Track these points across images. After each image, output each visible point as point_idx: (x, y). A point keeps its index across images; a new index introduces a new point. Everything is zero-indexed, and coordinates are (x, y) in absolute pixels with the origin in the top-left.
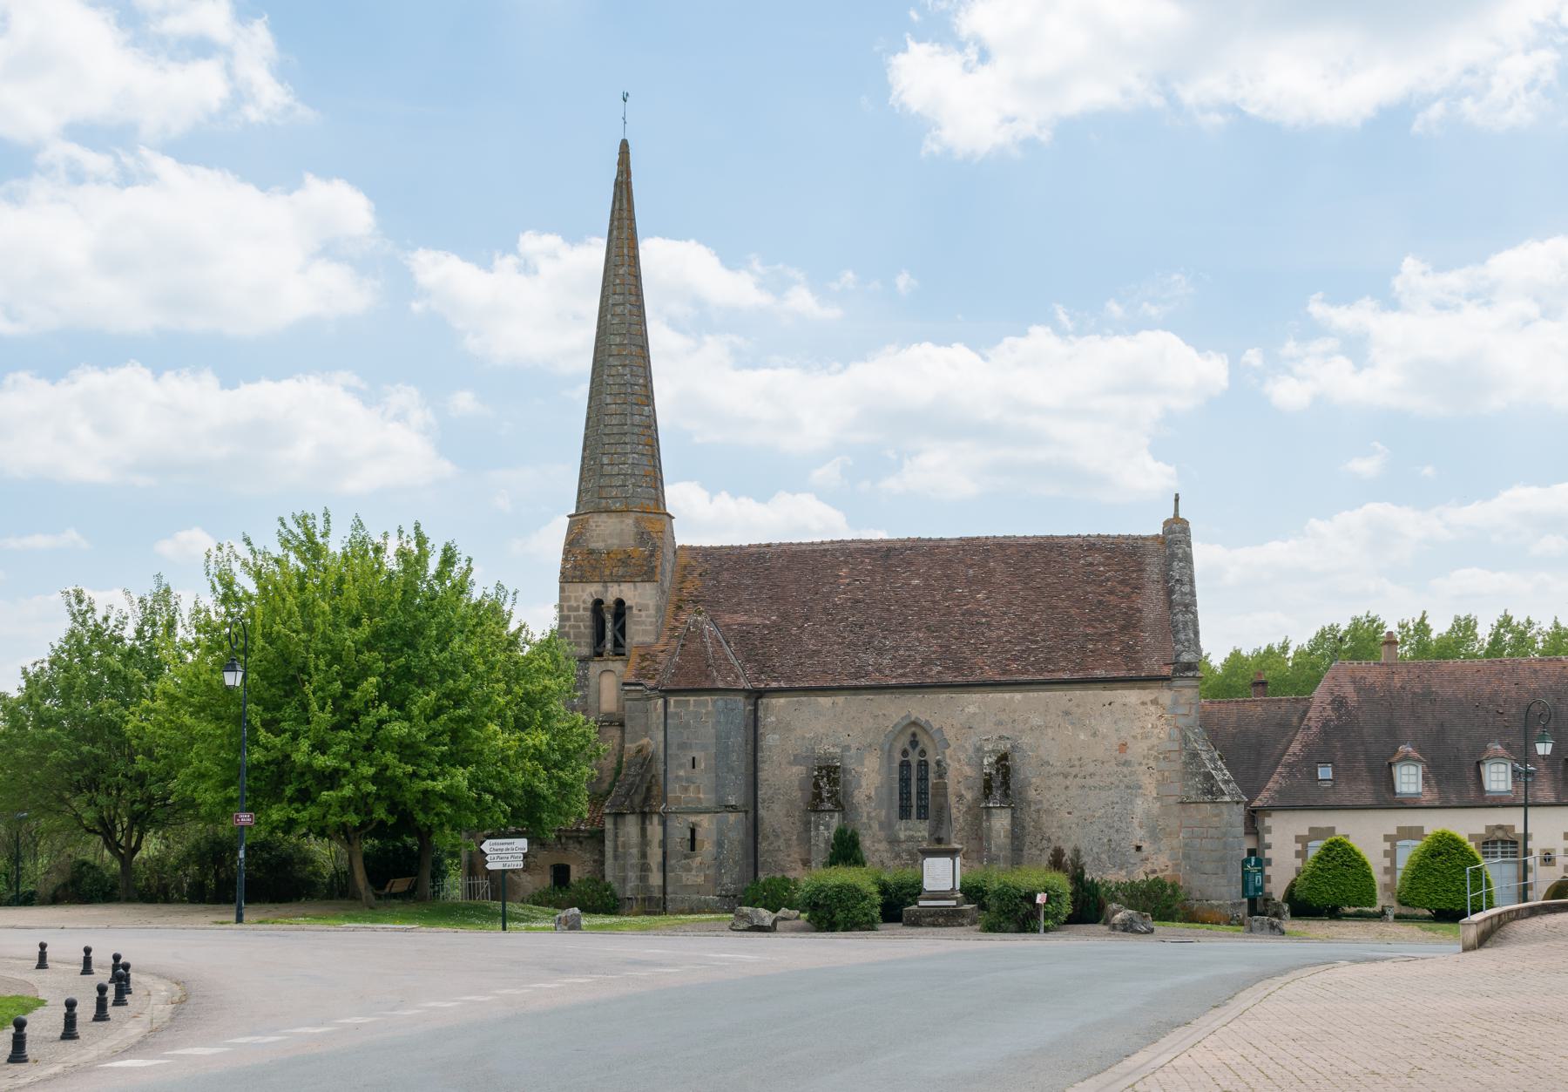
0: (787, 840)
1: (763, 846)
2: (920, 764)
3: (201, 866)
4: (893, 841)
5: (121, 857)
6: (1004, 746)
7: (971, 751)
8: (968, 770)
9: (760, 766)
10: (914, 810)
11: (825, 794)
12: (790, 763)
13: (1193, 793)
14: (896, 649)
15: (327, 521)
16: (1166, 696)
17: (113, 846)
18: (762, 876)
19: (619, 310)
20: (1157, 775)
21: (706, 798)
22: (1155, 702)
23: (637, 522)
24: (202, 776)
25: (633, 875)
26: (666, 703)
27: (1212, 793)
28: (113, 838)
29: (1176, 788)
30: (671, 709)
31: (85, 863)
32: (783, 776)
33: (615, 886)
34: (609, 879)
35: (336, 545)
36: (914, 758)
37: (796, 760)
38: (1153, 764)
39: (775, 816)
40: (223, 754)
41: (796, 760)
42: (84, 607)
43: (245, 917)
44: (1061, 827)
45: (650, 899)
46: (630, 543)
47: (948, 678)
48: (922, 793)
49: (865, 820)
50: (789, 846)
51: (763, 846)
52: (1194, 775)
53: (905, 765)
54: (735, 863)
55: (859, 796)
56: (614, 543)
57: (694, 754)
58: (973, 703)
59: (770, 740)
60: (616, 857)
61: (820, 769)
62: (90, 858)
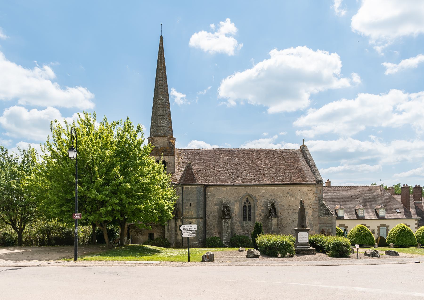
0: (214, 227)
1: (207, 228)
2: (249, 206)
3: (43, 234)
4: (243, 227)
5: (18, 232)
6: (272, 202)
7: (263, 202)
8: (262, 208)
9: (206, 206)
10: (247, 219)
11: (226, 214)
12: (215, 206)
13: (322, 215)
14: (241, 175)
15: (95, 116)
16: (314, 189)
17: (16, 229)
18: (207, 237)
19: (161, 82)
20: (312, 210)
21: (194, 215)
22: (311, 190)
23: (168, 140)
24: (50, 203)
25: (173, 236)
26: (182, 188)
27: (328, 214)
28: (15, 226)
29: (317, 213)
30: (184, 190)
31: (6, 234)
32: (213, 209)
33: (168, 239)
34: (166, 237)
35: (96, 126)
36: (247, 205)
37: (216, 205)
38: (311, 207)
39: (210, 220)
40: (60, 194)
41: (216, 205)
42: (4, 152)
43: (78, 259)
44: (287, 223)
45: (178, 243)
46: (166, 145)
47: (257, 183)
48: (250, 214)
49: (235, 221)
50: (214, 228)
51: (207, 228)
52: (322, 210)
53: (245, 206)
54: (202, 233)
55: (233, 215)
56: (162, 145)
57: (190, 202)
58: (264, 190)
59: (209, 199)
60: (168, 231)
61: (224, 207)
62: (8, 232)
